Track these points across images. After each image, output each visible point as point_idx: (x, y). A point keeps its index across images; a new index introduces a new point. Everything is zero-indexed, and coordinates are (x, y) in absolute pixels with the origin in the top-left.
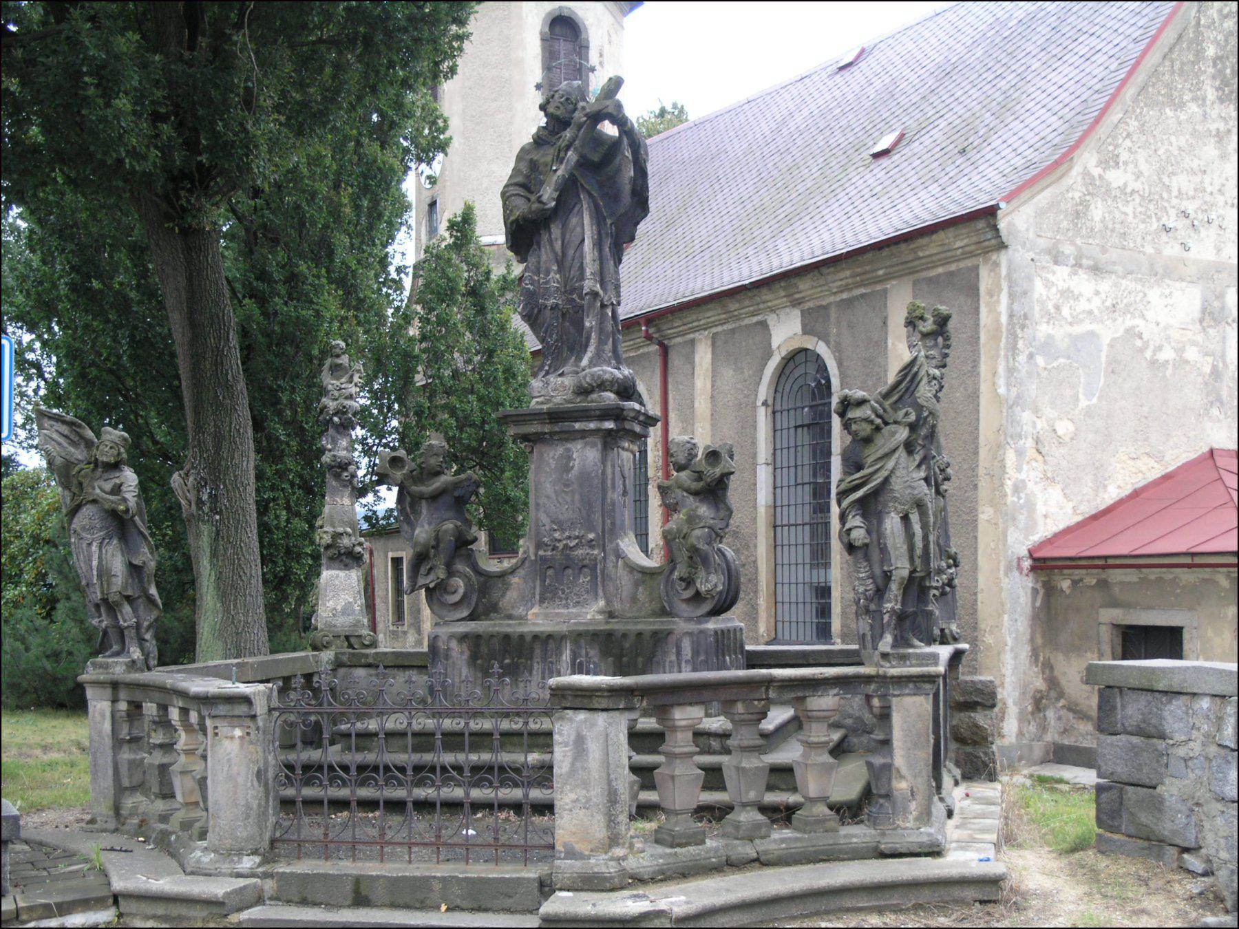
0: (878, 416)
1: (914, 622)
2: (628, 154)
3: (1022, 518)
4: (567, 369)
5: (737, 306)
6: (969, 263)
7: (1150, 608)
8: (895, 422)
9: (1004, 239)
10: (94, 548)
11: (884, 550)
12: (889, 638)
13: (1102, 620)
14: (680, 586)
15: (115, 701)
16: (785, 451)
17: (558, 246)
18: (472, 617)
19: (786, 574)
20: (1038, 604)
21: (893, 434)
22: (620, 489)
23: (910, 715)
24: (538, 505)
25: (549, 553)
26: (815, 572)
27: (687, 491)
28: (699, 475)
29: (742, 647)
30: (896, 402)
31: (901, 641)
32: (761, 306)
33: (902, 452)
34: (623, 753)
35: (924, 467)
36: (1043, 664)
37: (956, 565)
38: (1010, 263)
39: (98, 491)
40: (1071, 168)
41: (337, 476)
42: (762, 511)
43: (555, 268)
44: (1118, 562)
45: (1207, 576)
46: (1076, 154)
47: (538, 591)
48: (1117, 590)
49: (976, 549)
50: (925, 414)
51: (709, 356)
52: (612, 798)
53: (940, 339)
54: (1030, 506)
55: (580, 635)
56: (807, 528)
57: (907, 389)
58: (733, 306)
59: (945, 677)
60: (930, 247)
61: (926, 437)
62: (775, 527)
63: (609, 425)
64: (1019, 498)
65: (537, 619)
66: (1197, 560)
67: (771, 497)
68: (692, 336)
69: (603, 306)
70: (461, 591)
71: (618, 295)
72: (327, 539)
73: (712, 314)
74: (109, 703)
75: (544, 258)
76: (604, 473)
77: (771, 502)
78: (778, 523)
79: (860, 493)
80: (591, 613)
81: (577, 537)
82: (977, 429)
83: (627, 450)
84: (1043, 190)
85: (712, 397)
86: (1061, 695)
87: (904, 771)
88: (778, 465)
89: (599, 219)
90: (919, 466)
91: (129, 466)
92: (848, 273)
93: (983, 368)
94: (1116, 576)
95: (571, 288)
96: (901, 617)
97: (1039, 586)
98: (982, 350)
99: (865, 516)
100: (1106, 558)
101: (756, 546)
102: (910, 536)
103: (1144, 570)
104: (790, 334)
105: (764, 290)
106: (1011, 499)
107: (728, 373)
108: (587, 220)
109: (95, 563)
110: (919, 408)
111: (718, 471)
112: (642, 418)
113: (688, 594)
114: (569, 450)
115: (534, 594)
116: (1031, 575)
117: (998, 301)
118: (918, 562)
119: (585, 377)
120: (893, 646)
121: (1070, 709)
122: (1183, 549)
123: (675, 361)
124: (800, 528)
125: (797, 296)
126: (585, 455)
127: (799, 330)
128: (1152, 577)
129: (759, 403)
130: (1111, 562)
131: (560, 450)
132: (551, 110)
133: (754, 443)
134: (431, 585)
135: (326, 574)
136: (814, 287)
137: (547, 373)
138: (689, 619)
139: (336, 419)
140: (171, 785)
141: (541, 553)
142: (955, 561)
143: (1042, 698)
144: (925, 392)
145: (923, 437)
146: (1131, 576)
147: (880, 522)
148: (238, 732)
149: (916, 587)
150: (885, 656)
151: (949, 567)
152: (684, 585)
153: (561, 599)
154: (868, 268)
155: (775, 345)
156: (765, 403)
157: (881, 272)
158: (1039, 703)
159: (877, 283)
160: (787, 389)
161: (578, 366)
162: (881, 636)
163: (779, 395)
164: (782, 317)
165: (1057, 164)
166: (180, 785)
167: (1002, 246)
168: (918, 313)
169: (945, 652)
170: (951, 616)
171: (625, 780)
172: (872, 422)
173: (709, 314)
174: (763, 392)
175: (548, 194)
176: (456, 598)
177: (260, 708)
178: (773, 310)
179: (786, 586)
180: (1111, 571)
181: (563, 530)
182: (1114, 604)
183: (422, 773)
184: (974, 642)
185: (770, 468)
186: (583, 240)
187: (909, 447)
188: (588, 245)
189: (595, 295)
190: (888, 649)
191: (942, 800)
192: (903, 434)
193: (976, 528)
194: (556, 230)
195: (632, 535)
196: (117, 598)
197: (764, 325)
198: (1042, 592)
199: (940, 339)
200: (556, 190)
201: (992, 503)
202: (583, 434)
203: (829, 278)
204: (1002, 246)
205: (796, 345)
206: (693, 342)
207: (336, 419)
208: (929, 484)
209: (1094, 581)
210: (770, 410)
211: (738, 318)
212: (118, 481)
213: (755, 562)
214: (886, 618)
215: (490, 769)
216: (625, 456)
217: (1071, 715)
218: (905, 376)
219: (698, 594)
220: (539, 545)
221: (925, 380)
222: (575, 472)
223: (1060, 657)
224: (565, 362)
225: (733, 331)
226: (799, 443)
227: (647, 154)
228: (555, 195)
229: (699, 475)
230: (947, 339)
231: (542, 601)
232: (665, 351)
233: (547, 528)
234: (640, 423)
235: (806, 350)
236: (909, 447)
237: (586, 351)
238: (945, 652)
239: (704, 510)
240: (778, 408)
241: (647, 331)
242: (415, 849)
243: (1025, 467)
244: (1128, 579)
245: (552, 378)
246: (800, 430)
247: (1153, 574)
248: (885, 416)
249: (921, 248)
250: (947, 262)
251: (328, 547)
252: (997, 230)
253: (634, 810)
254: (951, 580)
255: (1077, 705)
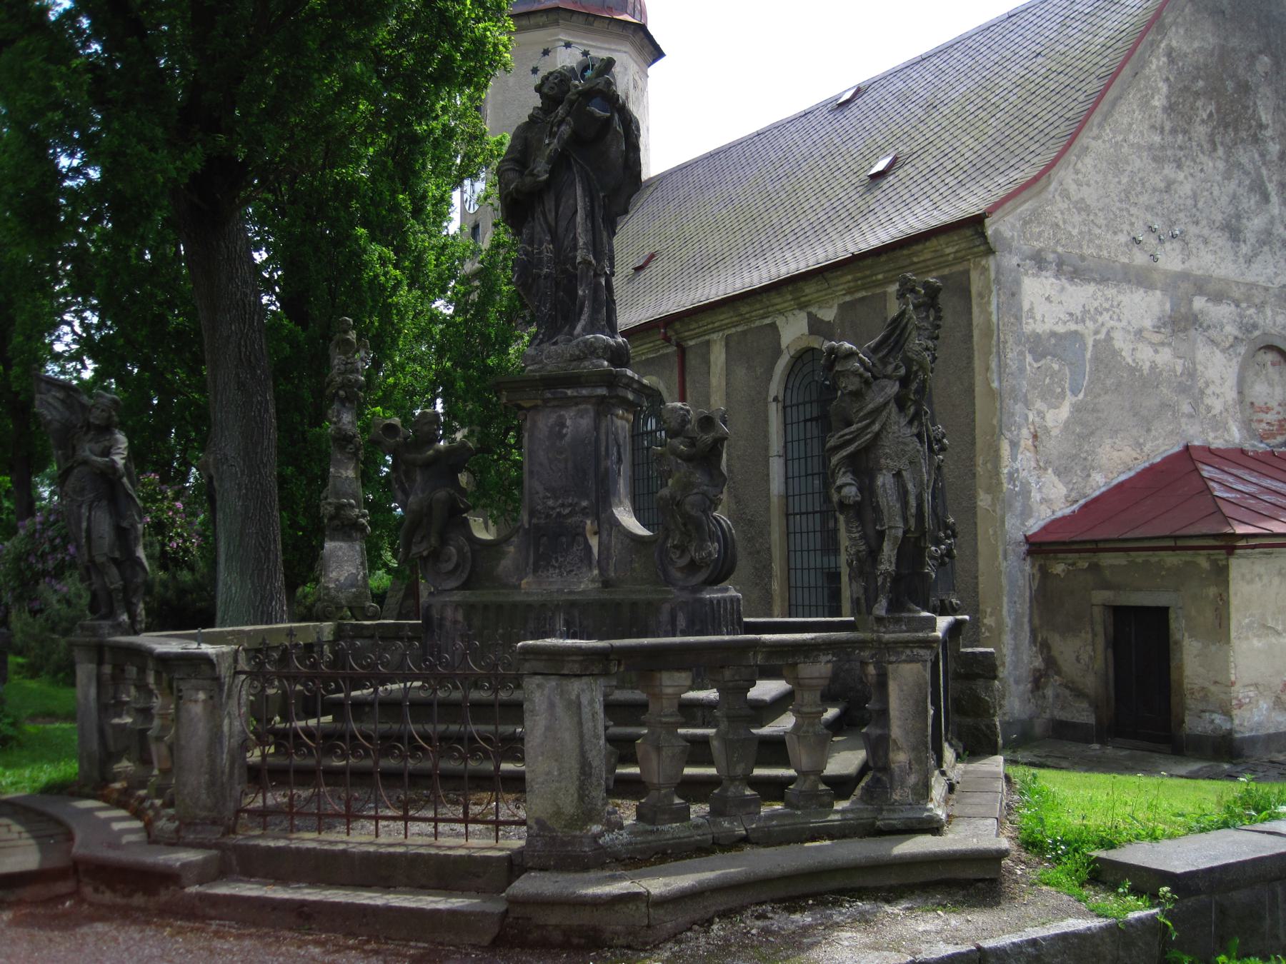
0: (867, 369)
1: (911, 588)
2: (620, 129)
3: (1018, 505)
4: (560, 338)
5: (748, 309)
6: (959, 268)
7: (1139, 590)
8: (885, 377)
9: (992, 245)
10: (84, 510)
11: (877, 509)
12: (884, 602)
13: (1094, 601)
14: (674, 556)
15: (100, 663)
16: (796, 444)
17: (551, 217)
18: (465, 586)
19: (798, 541)
20: (1034, 588)
21: (883, 389)
22: (614, 457)
23: (905, 682)
24: (531, 472)
25: (543, 521)
26: (825, 559)
27: (680, 457)
28: (692, 442)
29: (740, 619)
30: (884, 357)
31: (896, 605)
32: (770, 309)
33: (893, 408)
34: (596, 722)
35: (916, 423)
36: (1041, 645)
37: (954, 535)
38: (998, 267)
39: (87, 453)
40: (1049, 184)
41: (342, 448)
42: (775, 500)
43: (548, 238)
44: (1108, 546)
45: (1188, 559)
46: (1052, 172)
47: (531, 561)
48: (1107, 573)
49: (976, 535)
50: (915, 368)
51: (723, 356)
52: (585, 768)
53: (932, 312)
54: (1026, 493)
55: (573, 604)
56: (817, 515)
57: (897, 342)
58: (744, 310)
59: (944, 643)
60: (925, 253)
61: (916, 392)
62: (787, 515)
63: (602, 391)
64: (1015, 486)
65: (530, 588)
66: (1180, 543)
67: (782, 488)
68: (707, 337)
69: (596, 275)
70: (454, 559)
71: (612, 266)
72: (331, 509)
73: (724, 317)
74: (93, 667)
75: (538, 229)
76: (597, 440)
77: (782, 491)
78: (791, 511)
79: (844, 453)
80: (585, 583)
81: (570, 505)
82: (974, 421)
83: (622, 418)
84: (1025, 202)
85: (727, 394)
86: (1059, 673)
87: (901, 741)
88: (790, 457)
89: (590, 194)
90: (910, 423)
91: (121, 429)
92: (850, 277)
93: (978, 363)
94: (1107, 560)
95: (563, 256)
96: (897, 579)
97: (1035, 571)
98: (976, 347)
99: (856, 473)
100: (1096, 542)
101: (769, 534)
102: (903, 494)
103: (1132, 554)
104: (798, 334)
105: (773, 293)
106: (1006, 486)
107: (741, 372)
108: (579, 192)
109: (84, 525)
110: (908, 362)
111: (708, 438)
112: (635, 386)
113: (683, 562)
114: (561, 417)
115: (527, 564)
116: (1028, 559)
117: (989, 303)
118: (912, 522)
119: (578, 345)
120: (888, 611)
121: (1067, 687)
122: (1168, 533)
123: (692, 361)
124: (811, 516)
125: (803, 299)
126: (577, 422)
127: (806, 331)
128: (1140, 560)
129: (770, 399)
130: (1101, 545)
131: (552, 419)
132: (545, 90)
133: (766, 436)
134: (425, 553)
135: (329, 545)
136: (818, 291)
137: (542, 342)
138: (683, 589)
139: (342, 393)
140: (150, 754)
141: (535, 521)
142: (953, 531)
143: (1041, 676)
144: (916, 343)
145: (913, 396)
146: (1118, 560)
147: (873, 479)
148: (201, 696)
149: (911, 551)
150: (879, 620)
151: (948, 537)
152: (678, 553)
153: (555, 567)
154: (868, 273)
155: (783, 346)
156: (776, 399)
157: (880, 277)
158: (1038, 681)
159: (876, 286)
160: (797, 384)
161: (572, 335)
162: (876, 601)
163: (789, 392)
164: (791, 318)
165: (1036, 179)
166: (158, 752)
167: (990, 251)
168: (909, 286)
169: (943, 622)
170: (952, 588)
171: (598, 751)
172: (861, 376)
173: (722, 317)
174: (775, 388)
175: (541, 169)
176: (450, 566)
177: (224, 670)
178: (781, 313)
179: (799, 572)
180: (1101, 555)
181: (556, 498)
182: (1106, 586)
183: (388, 743)
184: (975, 611)
185: (782, 460)
186: (576, 211)
187: (901, 402)
188: (579, 218)
189: (586, 263)
190: (883, 613)
191: (943, 773)
192: (893, 388)
193: (975, 514)
194: (550, 204)
195: (627, 503)
196: (103, 559)
197: (773, 326)
198: (1038, 576)
199: (932, 312)
200: (548, 163)
201: (989, 490)
202: (576, 401)
203: (832, 282)
204: (990, 251)
205: (803, 344)
206: (708, 343)
207: (342, 393)
208: (921, 441)
209: (1086, 565)
210: (780, 405)
211: (749, 321)
212: (106, 443)
213: (769, 549)
214: (880, 580)
215: (459, 739)
216: (621, 423)
217: (1067, 692)
218: (893, 330)
219: (692, 561)
220: (532, 513)
221: (914, 333)
222: (568, 439)
223: (1057, 637)
224: (558, 331)
225: (744, 333)
226: (809, 436)
227: (638, 130)
228: (548, 167)
229: (692, 442)
230: (938, 310)
231: (535, 571)
232: (682, 352)
233: (541, 496)
234: (634, 391)
235: (813, 349)
236: (901, 402)
237: (579, 320)
238: (943, 622)
239: (698, 477)
240: (788, 403)
241: (665, 333)
242: (382, 823)
243: (1019, 457)
244: (1116, 562)
245: (545, 346)
246: (809, 424)
247: (1140, 557)
248: (874, 370)
249: (915, 254)
250: (939, 266)
251: (332, 518)
252: (985, 237)
253: (611, 783)
254: (949, 553)
255: (1073, 683)
